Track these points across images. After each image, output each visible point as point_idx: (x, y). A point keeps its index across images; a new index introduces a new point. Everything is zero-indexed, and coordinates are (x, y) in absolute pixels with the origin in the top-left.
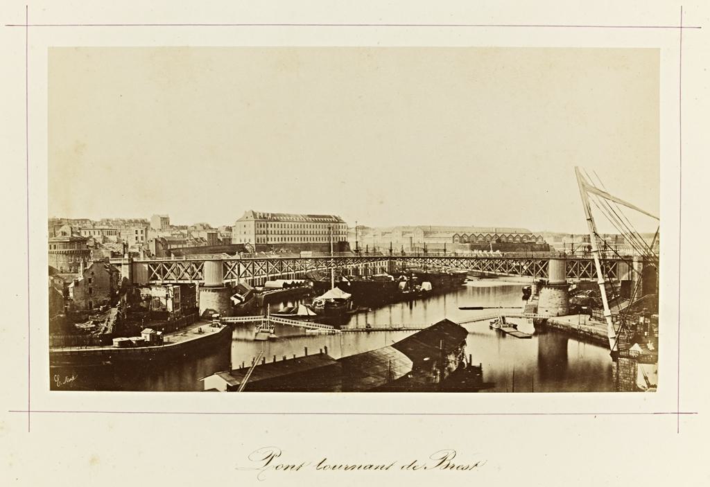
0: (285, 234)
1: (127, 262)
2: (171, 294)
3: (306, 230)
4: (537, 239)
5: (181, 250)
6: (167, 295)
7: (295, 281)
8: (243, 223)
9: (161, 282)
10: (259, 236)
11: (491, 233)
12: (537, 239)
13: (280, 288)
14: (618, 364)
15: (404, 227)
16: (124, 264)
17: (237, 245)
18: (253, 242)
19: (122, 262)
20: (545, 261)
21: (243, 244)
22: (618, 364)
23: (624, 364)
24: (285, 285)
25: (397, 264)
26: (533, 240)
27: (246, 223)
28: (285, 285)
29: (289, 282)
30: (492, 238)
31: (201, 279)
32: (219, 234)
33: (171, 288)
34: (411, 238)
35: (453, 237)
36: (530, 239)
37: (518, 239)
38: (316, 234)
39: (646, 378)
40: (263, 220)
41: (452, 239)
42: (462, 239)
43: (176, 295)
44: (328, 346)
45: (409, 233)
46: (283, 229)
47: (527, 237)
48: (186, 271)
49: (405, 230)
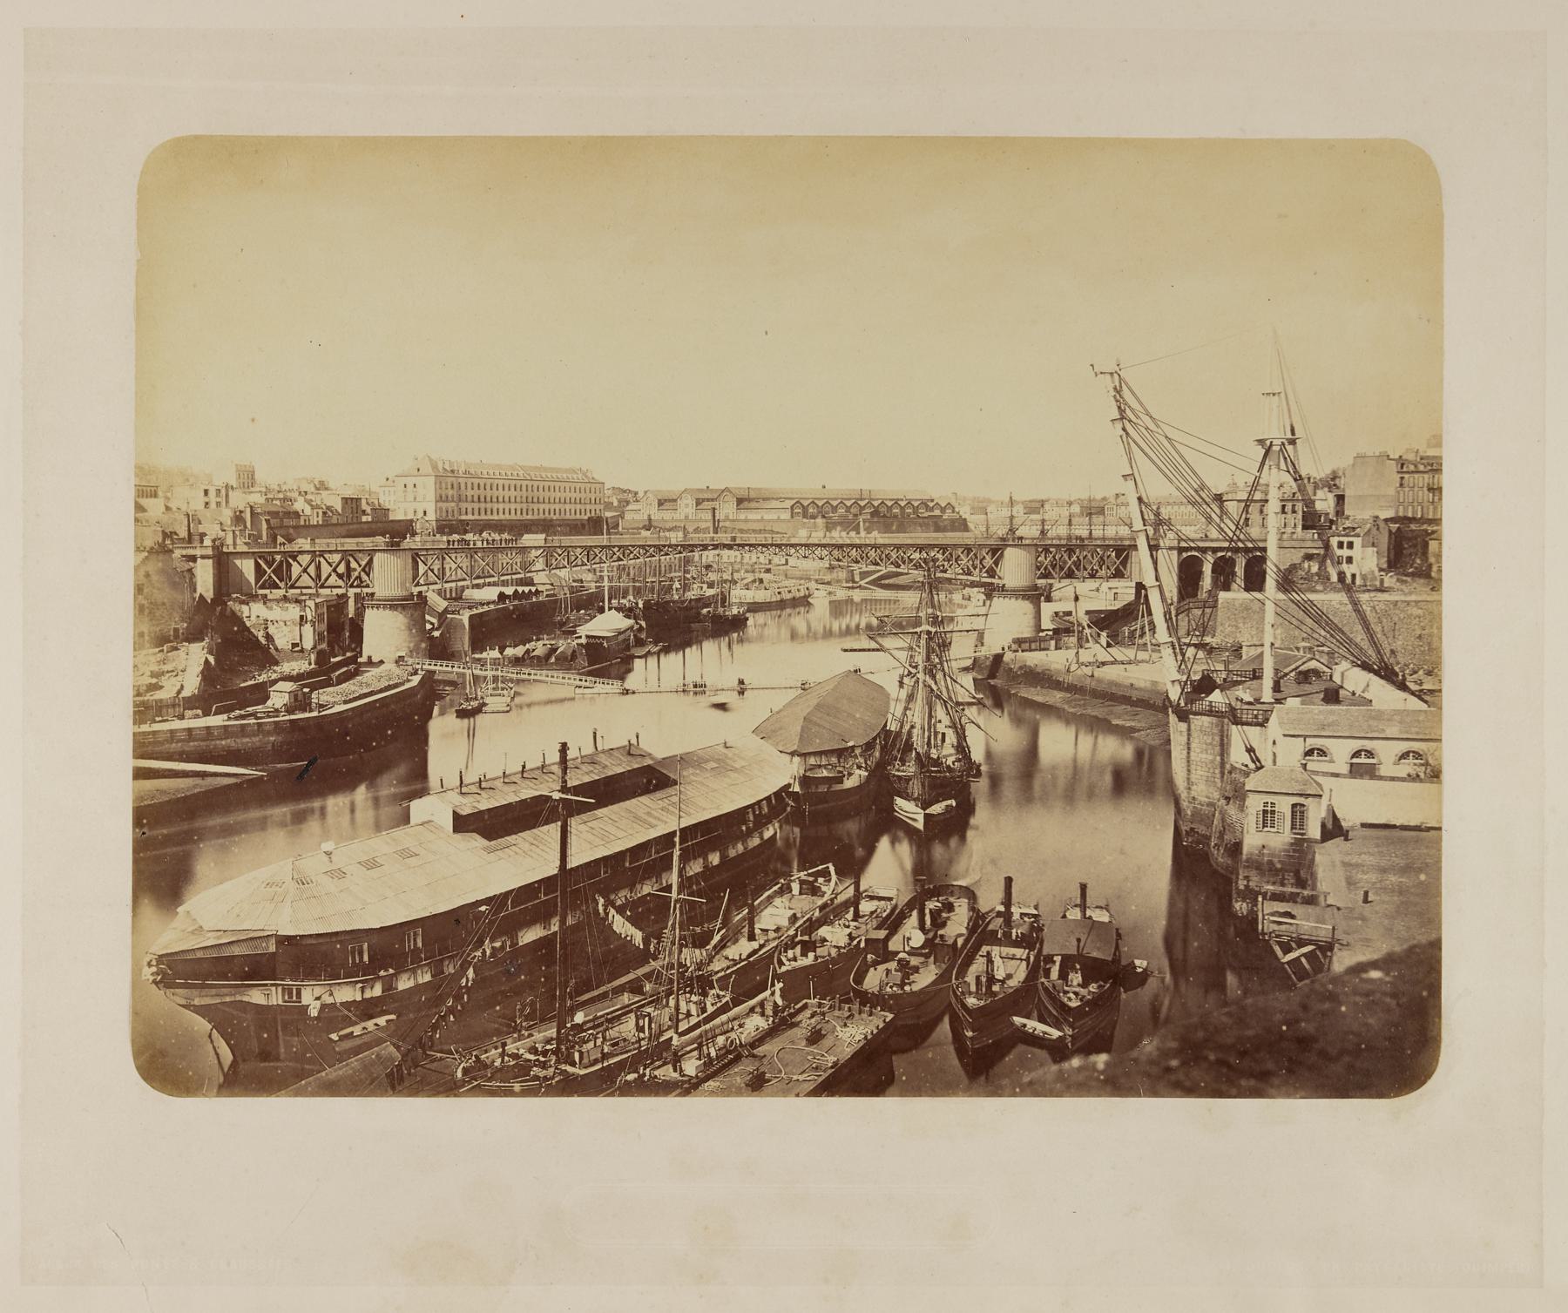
0: (560, 502)
1: (210, 552)
2: (310, 615)
3: (553, 495)
4: (943, 510)
5: (291, 531)
6: (302, 617)
7: (520, 589)
8: (410, 481)
9: (281, 592)
10: (444, 505)
11: (832, 499)
12: (943, 510)
13: (493, 602)
14: (1189, 726)
15: (700, 490)
16: (203, 557)
17: (400, 521)
18: (431, 516)
19: (198, 552)
20: (998, 550)
21: (412, 521)
22: (1189, 726)
23: (1201, 726)
24: (502, 597)
25: (697, 558)
26: (937, 512)
27: (418, 481)
28: (502, 597)
29: (509, 591)
30: (862, 508)
31: (368, 586)
32: (364, 502)
33: (311, 603)
34: (714, 509)
35: (792, 507)
36: (932, 509)
37: (842, 511)
38: (560, 502)
39: (1250, 750)
40: (451, 483)
41: (789, 511)
42: (803, 510)
43: (320, 617)
44: (383, 667)
45: (708, 500)
46: (489, 493)
47: (927, 506)
48: (305, 571)
49: (701, 496)
